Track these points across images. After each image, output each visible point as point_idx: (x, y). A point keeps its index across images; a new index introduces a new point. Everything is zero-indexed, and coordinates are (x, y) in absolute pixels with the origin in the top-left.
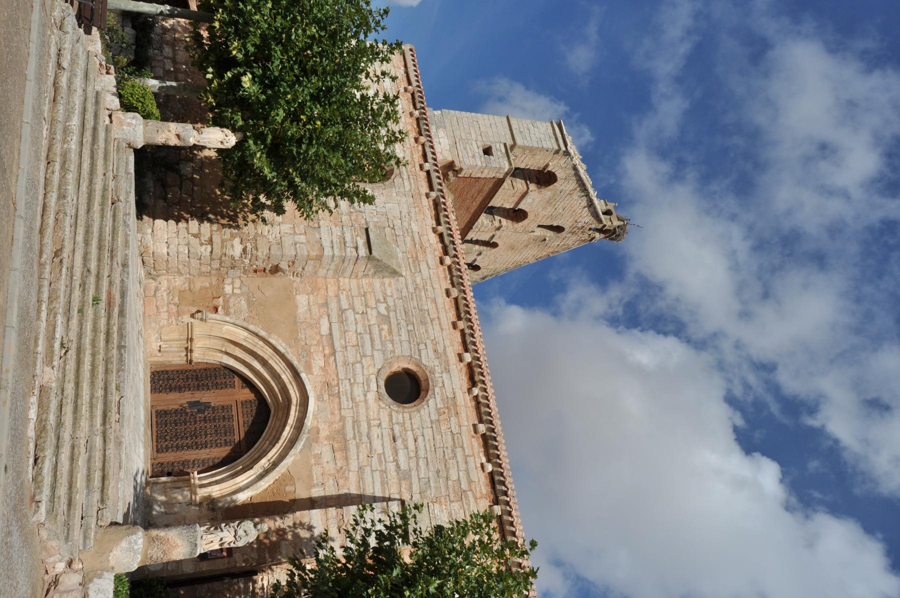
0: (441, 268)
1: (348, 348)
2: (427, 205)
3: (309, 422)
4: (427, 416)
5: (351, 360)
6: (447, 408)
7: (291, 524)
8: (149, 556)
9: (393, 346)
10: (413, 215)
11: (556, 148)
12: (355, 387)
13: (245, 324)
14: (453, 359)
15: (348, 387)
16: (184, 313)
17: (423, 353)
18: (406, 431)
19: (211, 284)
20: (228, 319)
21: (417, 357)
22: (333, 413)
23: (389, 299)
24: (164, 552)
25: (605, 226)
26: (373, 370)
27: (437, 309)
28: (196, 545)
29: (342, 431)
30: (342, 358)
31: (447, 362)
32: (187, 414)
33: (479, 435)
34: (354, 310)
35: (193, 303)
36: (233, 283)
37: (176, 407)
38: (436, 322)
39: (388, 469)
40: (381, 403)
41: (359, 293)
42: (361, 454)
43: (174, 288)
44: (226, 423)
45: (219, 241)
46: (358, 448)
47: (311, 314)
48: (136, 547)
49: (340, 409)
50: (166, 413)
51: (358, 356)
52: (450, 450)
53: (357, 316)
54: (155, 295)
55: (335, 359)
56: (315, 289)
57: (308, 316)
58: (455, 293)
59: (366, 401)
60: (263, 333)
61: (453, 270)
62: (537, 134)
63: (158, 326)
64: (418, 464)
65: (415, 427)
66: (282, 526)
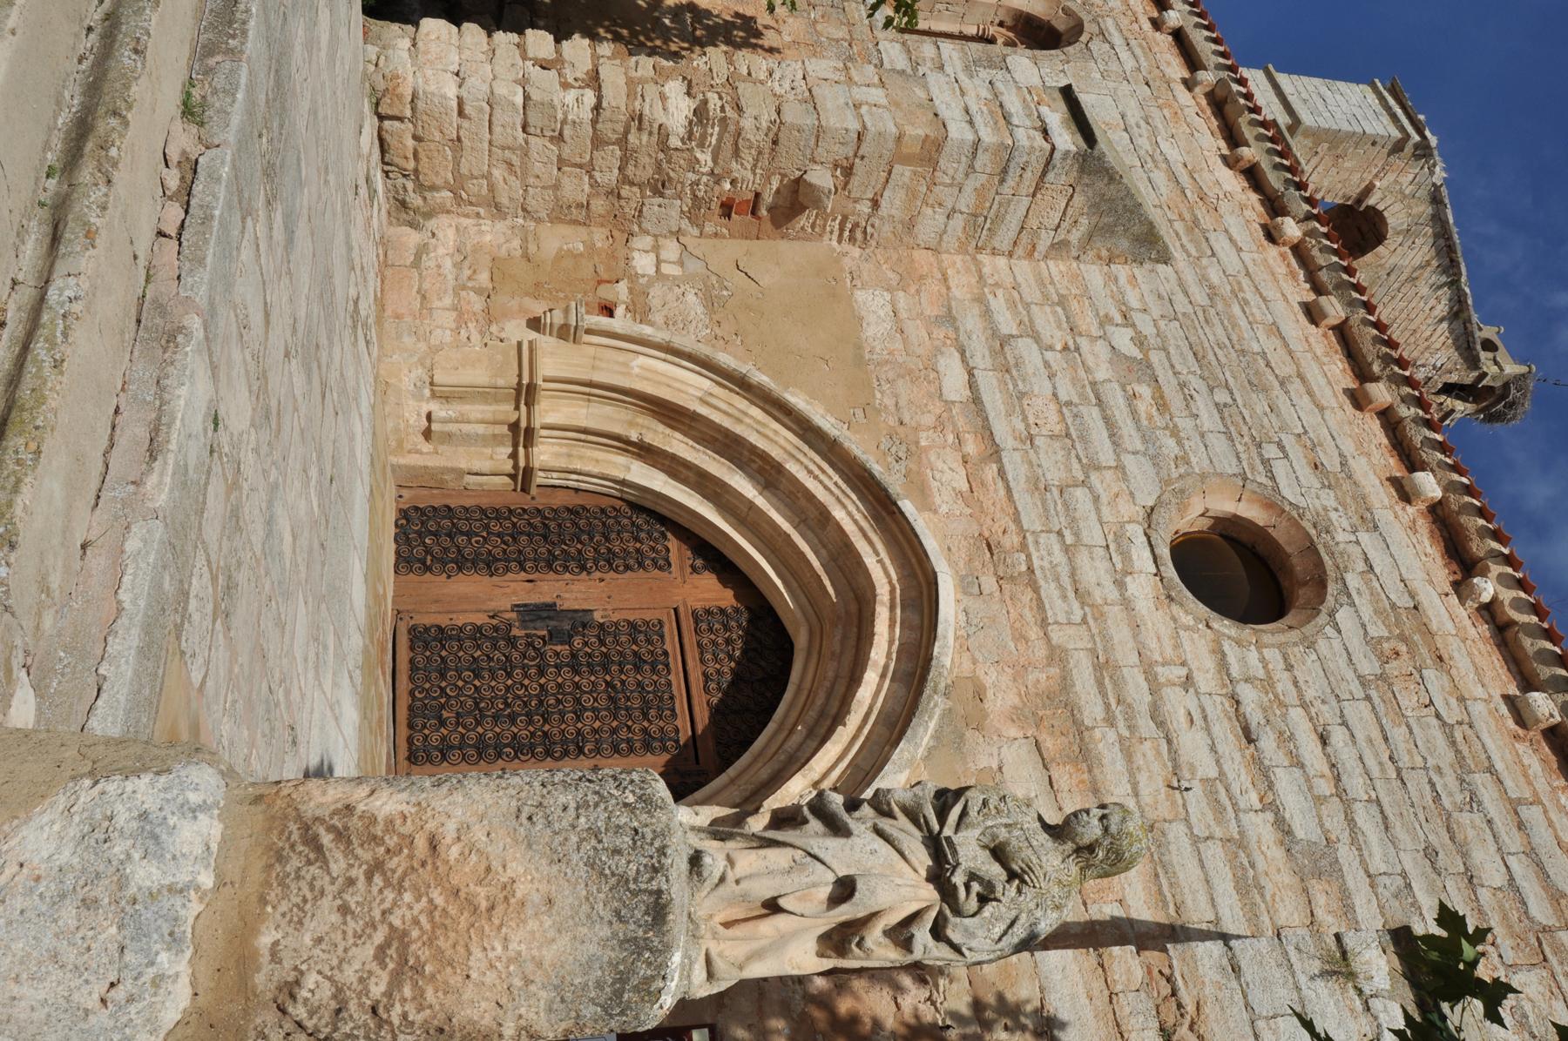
0: (1273, 251)
1: (1039, 441)
2: (1191, 105)
3: (946, 651)
4: (1342, 661)
5: (1054, 476)
6: (1403, 638)
7: (962, 1005)
8: (264, 980)
9: (1179, 443)
10: (1158, 122)
11: (1396, 134)
12: (1082, 559)
13: (704, 350)
14: (1381, 498)
15: (1059, 556)
16: (506, 315)
17: (1280, 468)
18: (1282, 704)
19: (590, 247)
20: (647, 331)
21: (1263, 480)
22: (1020, 637)
23: (1137, 317)
24: (398, 953)
25: (1484, 375)
26: (1127, 509)
27: (1290, 353)
28: (659, 911)
29: (1062, 696)
30: (1023, 469)
31: (1362, 500)
32: (512, 642)
33: (1535, 734)
34: (1037, 338)
35: (537, 290)
36: (656, 249)
37: (481, 619)
38: (1296, 386)
39: (1252, 835)
40: (1175, 608)
41: (1046, 297)
42: (1142, 778)
43: (477, 248)
44: (647, 678)
45: (622, 81)
46: (1128, 756)
47: (905, 341)
48: (145, 875)
49: (1044, 623)
50: (442, 634)
51: (1076, 466)
52: (1451, 779)
53: (1049, 355)
54: (417, 263)
55: (1002, 472)
56: (908, 279)
57: (899, 345)
58: (1334, 309)
59: (1127, 604)
60: (760, 378)
61: (1315, 252)
62: (1344, 106)
63: (422, 346)
64: (1351, 821)
65: (1310, 694)
66: (928, 1015)
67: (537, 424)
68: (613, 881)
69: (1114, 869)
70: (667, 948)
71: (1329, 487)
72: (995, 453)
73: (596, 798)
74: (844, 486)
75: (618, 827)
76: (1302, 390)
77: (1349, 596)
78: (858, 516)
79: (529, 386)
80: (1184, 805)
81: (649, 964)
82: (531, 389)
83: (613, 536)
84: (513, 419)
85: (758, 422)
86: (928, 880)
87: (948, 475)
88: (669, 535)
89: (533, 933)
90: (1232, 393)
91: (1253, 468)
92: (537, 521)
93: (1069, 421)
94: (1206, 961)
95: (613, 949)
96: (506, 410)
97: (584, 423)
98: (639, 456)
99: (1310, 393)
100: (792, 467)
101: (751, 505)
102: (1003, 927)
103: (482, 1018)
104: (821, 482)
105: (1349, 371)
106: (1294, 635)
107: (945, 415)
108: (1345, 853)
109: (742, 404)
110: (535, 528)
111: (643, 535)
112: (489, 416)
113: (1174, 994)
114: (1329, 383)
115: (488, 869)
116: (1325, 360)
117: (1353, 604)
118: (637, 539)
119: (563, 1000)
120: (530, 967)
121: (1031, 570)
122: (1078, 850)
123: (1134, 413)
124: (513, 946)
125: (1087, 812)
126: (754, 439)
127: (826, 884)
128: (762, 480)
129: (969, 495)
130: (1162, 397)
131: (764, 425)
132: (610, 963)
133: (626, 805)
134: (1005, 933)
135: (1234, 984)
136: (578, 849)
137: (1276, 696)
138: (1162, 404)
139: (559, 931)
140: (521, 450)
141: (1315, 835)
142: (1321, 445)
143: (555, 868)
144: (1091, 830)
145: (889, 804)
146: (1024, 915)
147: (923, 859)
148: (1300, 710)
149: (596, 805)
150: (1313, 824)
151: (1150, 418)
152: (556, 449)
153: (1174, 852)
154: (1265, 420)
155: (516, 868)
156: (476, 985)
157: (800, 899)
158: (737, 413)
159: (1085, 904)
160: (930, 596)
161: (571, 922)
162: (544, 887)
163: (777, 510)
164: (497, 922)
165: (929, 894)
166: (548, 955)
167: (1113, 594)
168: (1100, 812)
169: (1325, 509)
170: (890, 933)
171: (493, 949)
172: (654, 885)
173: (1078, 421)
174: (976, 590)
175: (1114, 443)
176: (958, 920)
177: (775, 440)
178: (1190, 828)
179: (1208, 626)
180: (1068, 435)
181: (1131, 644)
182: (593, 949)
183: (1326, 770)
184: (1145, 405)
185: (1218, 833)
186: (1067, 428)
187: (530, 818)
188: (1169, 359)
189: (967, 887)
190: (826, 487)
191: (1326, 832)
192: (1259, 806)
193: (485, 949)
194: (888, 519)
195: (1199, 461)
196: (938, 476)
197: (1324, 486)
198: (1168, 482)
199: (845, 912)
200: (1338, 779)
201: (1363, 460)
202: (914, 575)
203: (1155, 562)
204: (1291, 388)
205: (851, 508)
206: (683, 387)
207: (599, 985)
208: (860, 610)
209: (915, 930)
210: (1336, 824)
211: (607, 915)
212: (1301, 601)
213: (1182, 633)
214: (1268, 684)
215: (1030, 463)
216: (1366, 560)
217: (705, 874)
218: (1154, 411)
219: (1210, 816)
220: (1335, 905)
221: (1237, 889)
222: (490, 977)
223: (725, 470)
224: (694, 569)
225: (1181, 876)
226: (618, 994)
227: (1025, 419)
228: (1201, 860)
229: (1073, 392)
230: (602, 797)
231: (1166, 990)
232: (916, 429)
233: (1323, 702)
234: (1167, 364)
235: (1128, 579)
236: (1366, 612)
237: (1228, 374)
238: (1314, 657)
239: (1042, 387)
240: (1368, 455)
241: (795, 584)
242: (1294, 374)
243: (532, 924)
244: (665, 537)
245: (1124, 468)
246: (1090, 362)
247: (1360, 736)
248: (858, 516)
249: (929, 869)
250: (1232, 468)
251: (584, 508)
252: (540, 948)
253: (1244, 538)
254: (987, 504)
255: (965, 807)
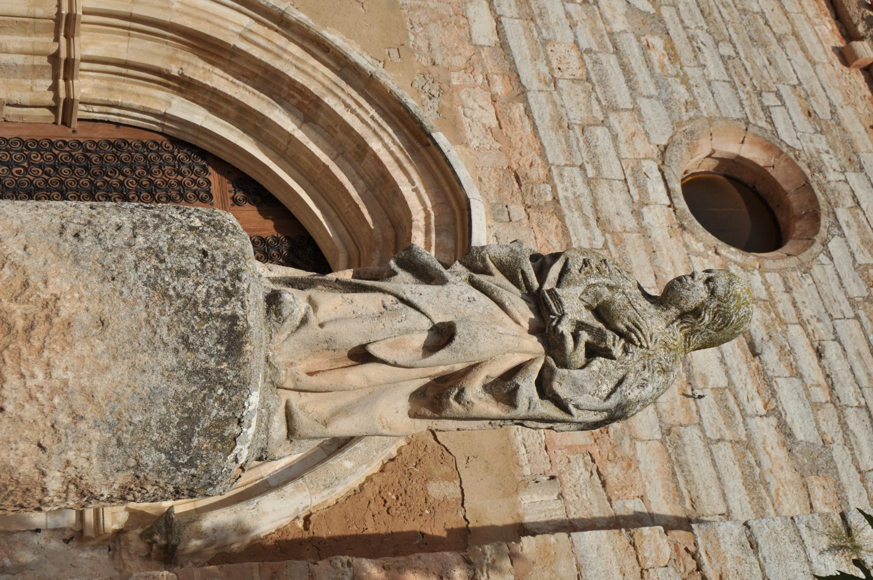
1: (561, 84)
4: (834, 285)
9: (689, 89)
12: (603, 190)
15: (582, 188)
17: (778, 115)
18: (782, 322)
21: (763, 123)
26: (642, 147)
27: (786, 13)
28: (234, 339)
30: (548, 109)
38: (791, 43)
39: (758, 437)
40: (687, 237)
51: (596, 107)
55: (528, 112)
59: (644, 232)
65: (807, 313)
67: (78, 54)
68: (179, 303)
69: (720, 336)
70: (244, 385)
71: (821, 132)
72: (522, 94)
73: (156, 221)
74: (380, 120)
75: (184, 248)
76: (797, 46)
77: (840, 228)
78: (394, 148)
79: (68, 16)
80: (698, 411)
81: (223, 403)
82: (71, 19)
83: (155, 169)
84: (53, 49)
85: (298, 59)
86: (531, 332)
87: (478, 113)
88: (210, 169)
89: (81, 358)
90: (735, 47)
91: (754, 114)
92: (78, 153)
93: (590, 66)
94: (727, 538)
95: (180, 382)
96: (46, 42)
97: (124, 56)
98: (180, 92)
99: (804, 49)
100: (330, 101)
101: (290, 137)
102: (611, 385)
103: (21, 463)
104: (358, 116)
105: (837, 32)
106: (792, 262)
107: (474, 58)
108: (839, 453)
109: (281, 41)
110: (77, 160)
111: (184, 168)
112: (28, 47)
113: (699, 568)
114: (820, 41)
115: (26, 285)
116: (817, 21)
117: (843, 235)
118: (179, 172)
119: (120, 444)
120: (79, 401)
121: (556, 199)
122: (682, 316)
123: (648, 61)
124: (57, 373)
125: (692, 276)
126: (292, 73)
127: (421, 331)
128: (301, 115)
129: (500, 129)
130: (673, 49)
131: (303, 61)
132: (176, 398)
133: (192, 228)
134: (613, 391)
135: (753, 559)
136: (136, 267)
137: (778, 315)
138: (673, 55)
139: (114, 358)
140: (61, 82)
141: (813, 437)
142: (814, 95)
143: (108, 286)
144: (698, 294)
145: (483, 260)
146: (631, 375)
147: (525, 313)
148: (798, 327)
149: (156, 227)
150: (811, 427)
151: (663, 66)
152: (97, 82)
153: (689, 453)
154: (765, 72)
155: (59, 284)
156: (12, 420)
157: (392, 346)
158: (276, 50)
159: (610, 500)
160: (463, 220)
161: (128, 348)
162: (94, 307)
163: (316, 143)
164: (37, 344)
165: (533, 346)
166: (101, 385)
167: (631, 222)
168: (706, 276)
169: (818, 152)
170: (490, 388)
171: (33, 376)
172: (228, 310)
173: (597, 67)
174: (505, 217)
175: (630, 88)
176: (565, 371)
177: (315, 76)
178: (703, 431)
179: (716, 253)
180: (588, 79)
181: (648, 268)
182: (155, 380)
183: (821, 379)
184: (658, 54)
185: (728, 435)
186: (588, 73)
187: (77, 235)
188: (679, 15)
189: (576, 337)
190: (363, 121)
191: (822, 434)
192: (763, 412)
193: (22, 376)
194: (423, 151)
195: (706, 106)
196: (468, 113)
197: (816, 132)
198: (679, 124)
199: (445, 361)
200: (832, 387)
201: (850, 110)
202: (448, 203)
203: (669, 194)
204: (787, 44)
205: (387, 140)
206: (223, 23)
207: (164, 426)
208: (396, 237)
209: (519, 380)
210: (831, 427)
211: (173, 341)
212: (797, 233)
213: (693, 258)
214: (770, 304)
215: (554, 103)
216: (854, 197)
217: (285, 313)
218: (666, 60)
219: (721, 421)
220: (831, 498)
221: (746, 485)
222: (30, 412)
223: (265, 105)
224: (235, 202)
225: (696, 473)
226: (186, 437)
227: (549, 63)
228: (713, 460)
229: (592, 41)
230: (163, 220)
231: (692, 565)
232: (448, 69)
233: (819, 320)
234: (677, 20)
235: (645, 210)
236: (855, 242)
237: (731, 30)
238: (810, 281)
239: (564, 35)
240: (854, 105)
241: (334, 214)
242: (789, 32)
243: (81, 348)
244: (206, 171)
245: (639, 110)
246: (608, 14)
247: (850, 350)
248: (394, 148)
249: (531, 322)
250: (735, 112)
251: (125, 142)
252: (90, 377)
253: (746, 178)
254: (515, 139)
255: (566, 264)
